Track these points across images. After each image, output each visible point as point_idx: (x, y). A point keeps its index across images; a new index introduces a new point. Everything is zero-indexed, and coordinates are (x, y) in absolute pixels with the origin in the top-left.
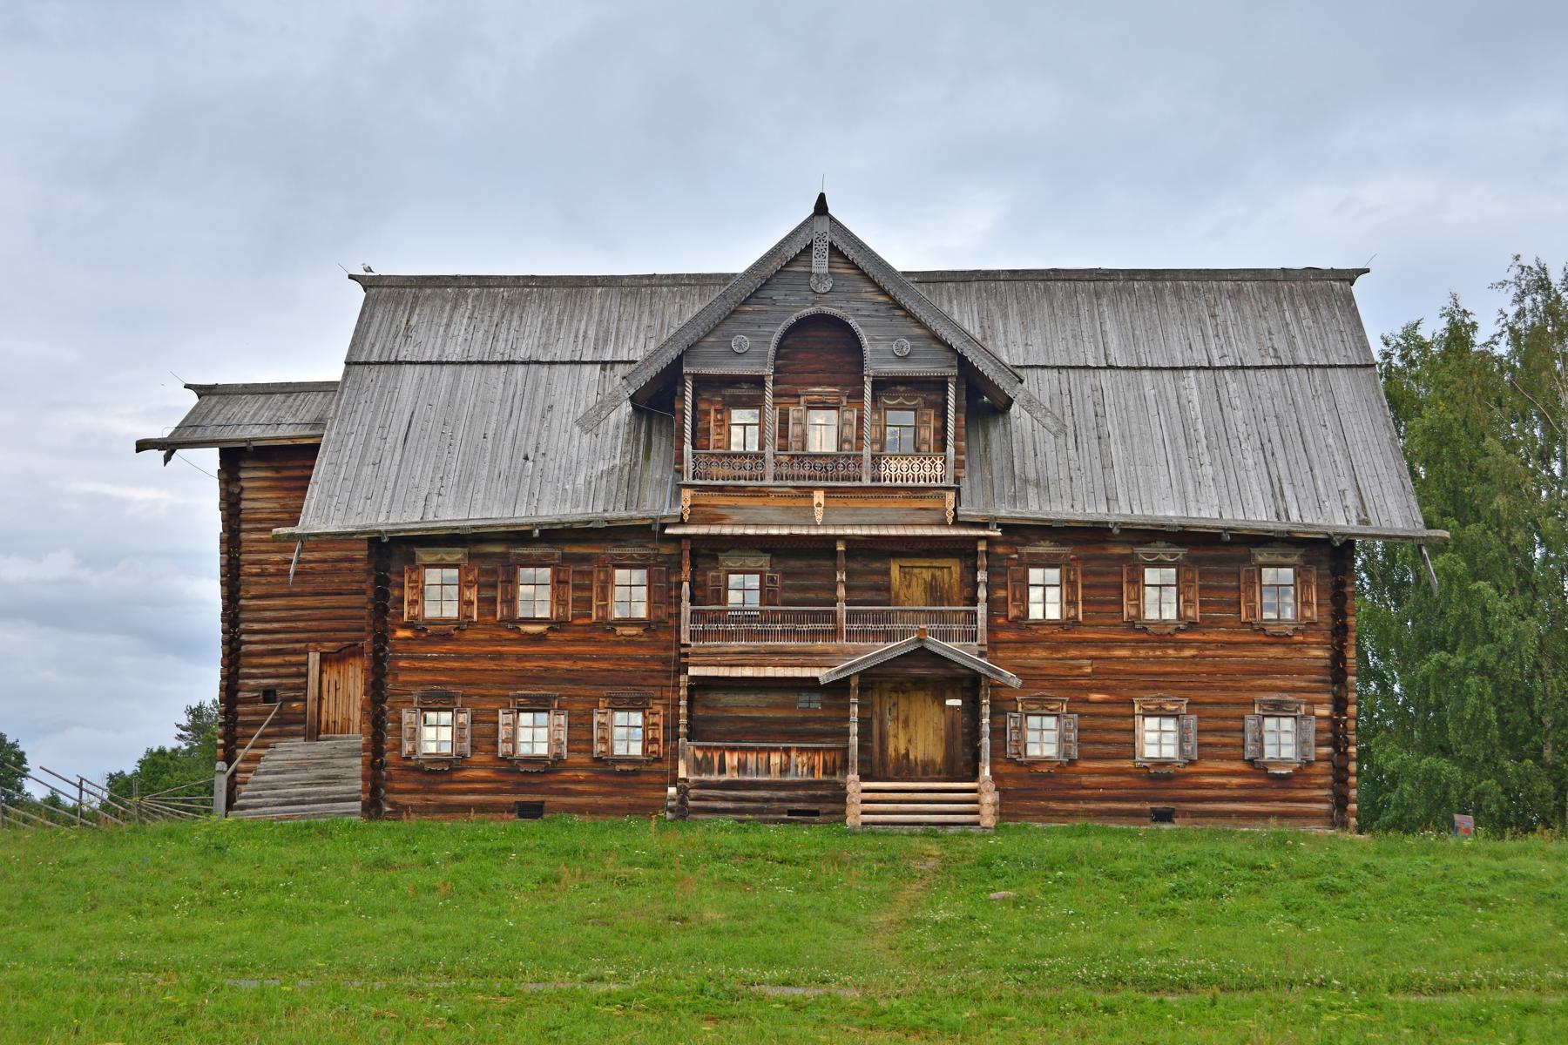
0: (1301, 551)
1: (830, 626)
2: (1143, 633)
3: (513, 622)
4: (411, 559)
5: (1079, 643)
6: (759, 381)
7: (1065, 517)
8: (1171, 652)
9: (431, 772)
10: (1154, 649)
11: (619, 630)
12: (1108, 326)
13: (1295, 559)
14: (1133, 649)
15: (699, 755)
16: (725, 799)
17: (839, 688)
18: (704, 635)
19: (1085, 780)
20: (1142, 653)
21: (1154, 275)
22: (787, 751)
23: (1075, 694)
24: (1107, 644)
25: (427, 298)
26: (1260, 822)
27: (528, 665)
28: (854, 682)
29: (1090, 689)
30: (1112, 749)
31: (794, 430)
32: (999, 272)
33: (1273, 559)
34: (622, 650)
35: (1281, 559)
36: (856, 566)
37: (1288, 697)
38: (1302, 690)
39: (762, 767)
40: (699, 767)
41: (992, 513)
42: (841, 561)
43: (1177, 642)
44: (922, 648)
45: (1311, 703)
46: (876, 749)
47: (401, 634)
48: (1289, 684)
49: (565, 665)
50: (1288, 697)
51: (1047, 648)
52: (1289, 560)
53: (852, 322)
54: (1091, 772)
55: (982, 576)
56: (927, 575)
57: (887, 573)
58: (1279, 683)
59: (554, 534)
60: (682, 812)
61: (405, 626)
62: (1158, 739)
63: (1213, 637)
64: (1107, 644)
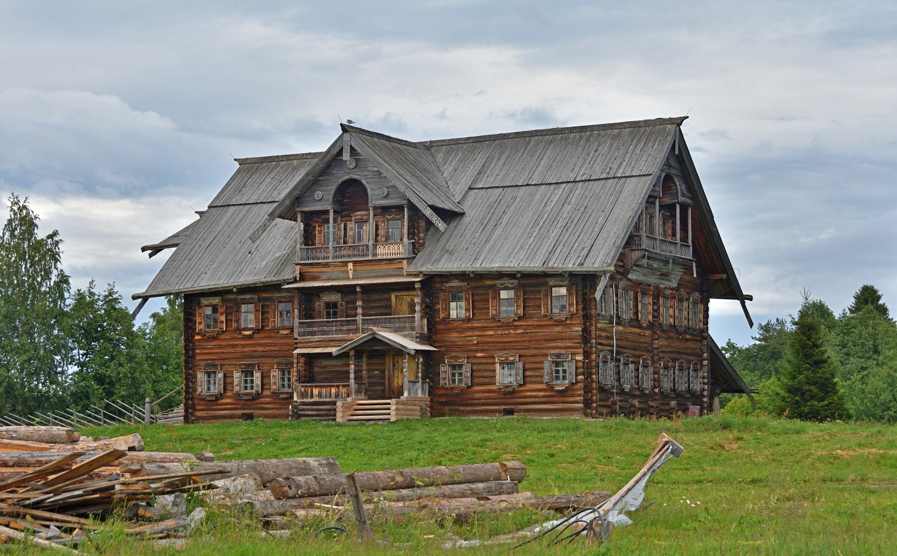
1: (354, 327)
2: (499, 323)
3: (239, 330)
4: (199, 304)
5: (473, 328)
7: (449, 270)
9: (209, 401)
10: (504, 330)
11: (281, 332)
13: (566, 283)
14: (496, 330)
15: (303, 390)
16: (312, 410)
17: (344, 355)
18: (304, 334)
20: (499, 332)
22: (338, 386)
23: (471, 354)
24: (484, 328)
25: (263, 168)
27: (246, 350)
28: (352, 353)
29: (477, 351)
30: (487, 380)
32: (510, 134)
33: (556, 283)
34: (283, 341)
35: (560, 283)
37: (563, 351)
38: (571, 348)
39: (328, 394)
40: (303, 395)
41: (420, 270)
42: (359, 296)
43: (515, 326)
44: (374, 337)
45: (573, 354)
46: (387, 384)
47: (197, 337)
48: (564, 345)
49: (260, 349)
50: (563, 351)
52: (564, 283)
54: (478, 392)
56: (409, 299)
57: (390, 299)
58: (560, 345)
60: (297, 416)
61: (199, 334)
62: (505, 377)
63: (530, 323)
64: (484, 328)
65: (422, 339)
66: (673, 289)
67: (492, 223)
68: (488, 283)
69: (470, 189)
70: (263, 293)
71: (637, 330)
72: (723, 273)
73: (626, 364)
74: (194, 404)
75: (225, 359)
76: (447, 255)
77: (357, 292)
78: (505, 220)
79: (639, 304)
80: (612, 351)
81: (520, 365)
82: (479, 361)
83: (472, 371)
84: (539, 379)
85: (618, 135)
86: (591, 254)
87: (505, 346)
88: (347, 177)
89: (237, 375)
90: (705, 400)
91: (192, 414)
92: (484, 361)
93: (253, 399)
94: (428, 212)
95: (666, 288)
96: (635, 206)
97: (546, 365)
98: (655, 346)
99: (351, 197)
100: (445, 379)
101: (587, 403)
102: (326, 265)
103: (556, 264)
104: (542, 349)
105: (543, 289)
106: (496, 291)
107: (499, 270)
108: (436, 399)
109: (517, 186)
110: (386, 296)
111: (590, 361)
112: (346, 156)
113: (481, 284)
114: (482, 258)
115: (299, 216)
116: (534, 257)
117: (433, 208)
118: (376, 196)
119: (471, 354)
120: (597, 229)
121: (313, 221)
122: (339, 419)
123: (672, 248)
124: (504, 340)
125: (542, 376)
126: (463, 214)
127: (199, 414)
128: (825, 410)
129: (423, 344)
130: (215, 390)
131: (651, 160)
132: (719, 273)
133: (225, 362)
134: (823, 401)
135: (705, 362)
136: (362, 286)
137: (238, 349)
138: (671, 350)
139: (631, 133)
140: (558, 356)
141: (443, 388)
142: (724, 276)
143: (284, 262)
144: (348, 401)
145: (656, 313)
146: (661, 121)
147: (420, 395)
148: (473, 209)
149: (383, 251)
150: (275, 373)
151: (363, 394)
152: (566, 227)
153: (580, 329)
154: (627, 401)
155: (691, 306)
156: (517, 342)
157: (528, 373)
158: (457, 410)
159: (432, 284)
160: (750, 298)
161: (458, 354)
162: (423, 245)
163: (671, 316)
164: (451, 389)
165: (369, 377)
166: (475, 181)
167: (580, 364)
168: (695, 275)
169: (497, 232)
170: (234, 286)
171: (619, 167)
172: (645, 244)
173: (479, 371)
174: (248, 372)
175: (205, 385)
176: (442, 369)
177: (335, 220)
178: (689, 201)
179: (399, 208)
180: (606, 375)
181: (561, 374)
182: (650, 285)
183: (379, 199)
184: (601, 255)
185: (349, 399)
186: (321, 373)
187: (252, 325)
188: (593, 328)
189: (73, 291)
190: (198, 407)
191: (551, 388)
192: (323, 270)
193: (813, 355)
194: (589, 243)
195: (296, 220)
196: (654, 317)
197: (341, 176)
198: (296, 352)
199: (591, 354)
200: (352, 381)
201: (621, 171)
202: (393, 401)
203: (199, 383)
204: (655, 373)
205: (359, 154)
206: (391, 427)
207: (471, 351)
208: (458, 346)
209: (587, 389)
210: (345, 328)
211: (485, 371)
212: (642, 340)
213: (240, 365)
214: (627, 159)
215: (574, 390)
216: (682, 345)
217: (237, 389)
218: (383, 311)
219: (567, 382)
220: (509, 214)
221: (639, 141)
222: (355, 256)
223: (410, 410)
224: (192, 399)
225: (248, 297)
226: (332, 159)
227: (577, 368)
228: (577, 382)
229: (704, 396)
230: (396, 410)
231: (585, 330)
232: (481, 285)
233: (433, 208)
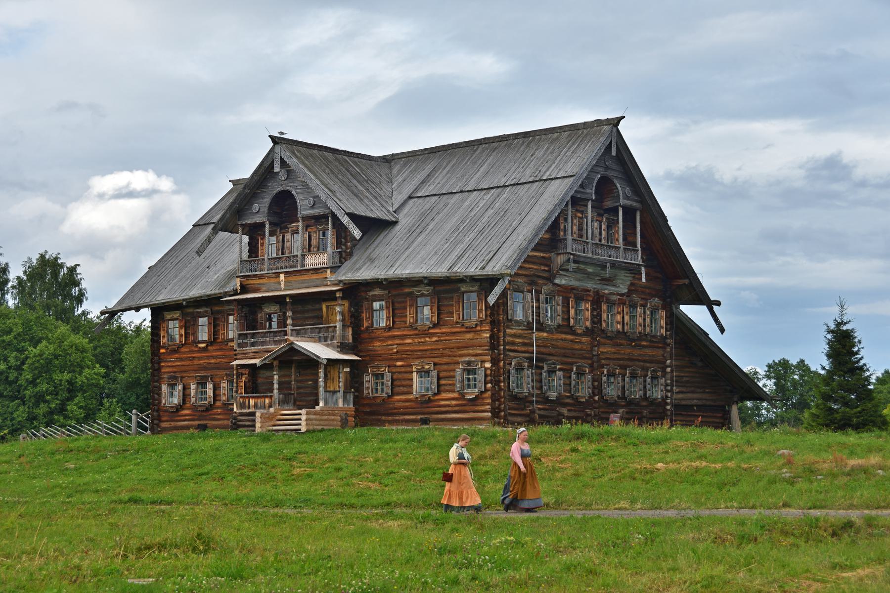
0: (478, 284)
5: (394, 337)
7: (365, 278)
8: (427, 339)
13: (476, 288)
14: (413, 339)
19: (397, 405)
20: (416, 340)
21: (526, 135)
23: (391, 363)
27: (202, 362)
28: (276, 363)
29: (397, 360)
31: (287, 244)
37: (473, 359)
40: (242, 406)
45: (483, 362)
47: (162, 351)
49: (213, 361)
50: (473, 359)
53: (293, 192)
54: (399, 401)
57: (321, 309)
58: (471, 352)
59: (433, 282)
61: (163, 347)
62: (419, 385)
63: (444, 330)
66: (622, 295)
67: (418, 230)
70: (211, 305)
71: (569, 337)
72: (685, 278)
73: (551, 372)
74: (159, 416)
75: (185, 371)
76: (369, 263)
77: (299, 302)
78: (430, 227)
79: (597, 308)
80: (531, 359)
81: (434, 373)
82: (399, 370)
85: (558, 138)
86: (495, 258)
87: (422, 355)
89: (193, 387)
90: (668, 407)
92: (403, 369)
94: (345, 220)
95: (610, 294)
97: (458, 373)
99: (284, 210)
100: (368, 388)
101: (495, 413)
102: (262, 277)
103: (461, 269)
104: (455, 356)
105: (455, 295)
106: (413, 297)
107: (408, 276)
109: (452, 193)
110: (317, 306)
112: (277, 168)
116: (443, 262)
118: (304, 208)
119: (391, 363)
121: (255, 232)
123: (612, 252)
124: (421, 348)
125: (454, 385)
127: (164, 425)
130: (176, 401)
131: (578, 161)
135: (669, 369)
136: (291, 296)
137: (196, 362)
138: (619, 356)
139: (569, 135)
140: (469, 363)
142: (686, 281)
143: (232, 275)
144: (265, 412)
145: (597, 318)
146: (599, 122)
147: (341, 404)
149: (312, 261)
150: (224, 384)
152: (481, 232)
153: (488, 335)
154: (554, 410)
155: (648, 312)
156: (432, 350)
157: (442, 382)
158: (379, 420)
159: (356, 293)
160: (718, 303)
161: (380, 364)
162: (351, 254)
163: (618, 323)
165: (298, 388)
166: (416, 190)
167: (489, 372)
168: (644, 280)
169: (420, 239)
170: (184, 300)
171: (548, 170)
173: (400, 379)
174: (202, 384)
175: (170, 397)
176: (366, 378)
177: (271, 234)
178: (635, 204)
179: (325, 217)
180: (524, 383)
182: (589, 291)
183: (306, 209)
185: (272, 410)
187: (206, 338)
190: (164, 419)
191: (462, 396)
192: (261, 281)
194: (498, 246)
195: (534, 250)
196: (593, 322)
197: (275, 188)
199: (499, 361)
200: (276, 391)
201: (548, 173)
202: (303, 411)
203: (163, 395)
205: (288, 166)
207: (392, 359)
209: (495, 398)
210: (277, 339)
212: (577, 346)
213: (196, 377)
214: (557, 162)
215: (483, 399)
216: (637, 352)
217: (193, 400)
219: (477, 390)
221: (573, 144)
222: (287, 267)
223: (326, 420)
224: (157, 411)
227: (486, 376)
228: (486, 390)
229: (667, 404)
230: (306, 420)
232: (398, 290)
233: (352, 216)
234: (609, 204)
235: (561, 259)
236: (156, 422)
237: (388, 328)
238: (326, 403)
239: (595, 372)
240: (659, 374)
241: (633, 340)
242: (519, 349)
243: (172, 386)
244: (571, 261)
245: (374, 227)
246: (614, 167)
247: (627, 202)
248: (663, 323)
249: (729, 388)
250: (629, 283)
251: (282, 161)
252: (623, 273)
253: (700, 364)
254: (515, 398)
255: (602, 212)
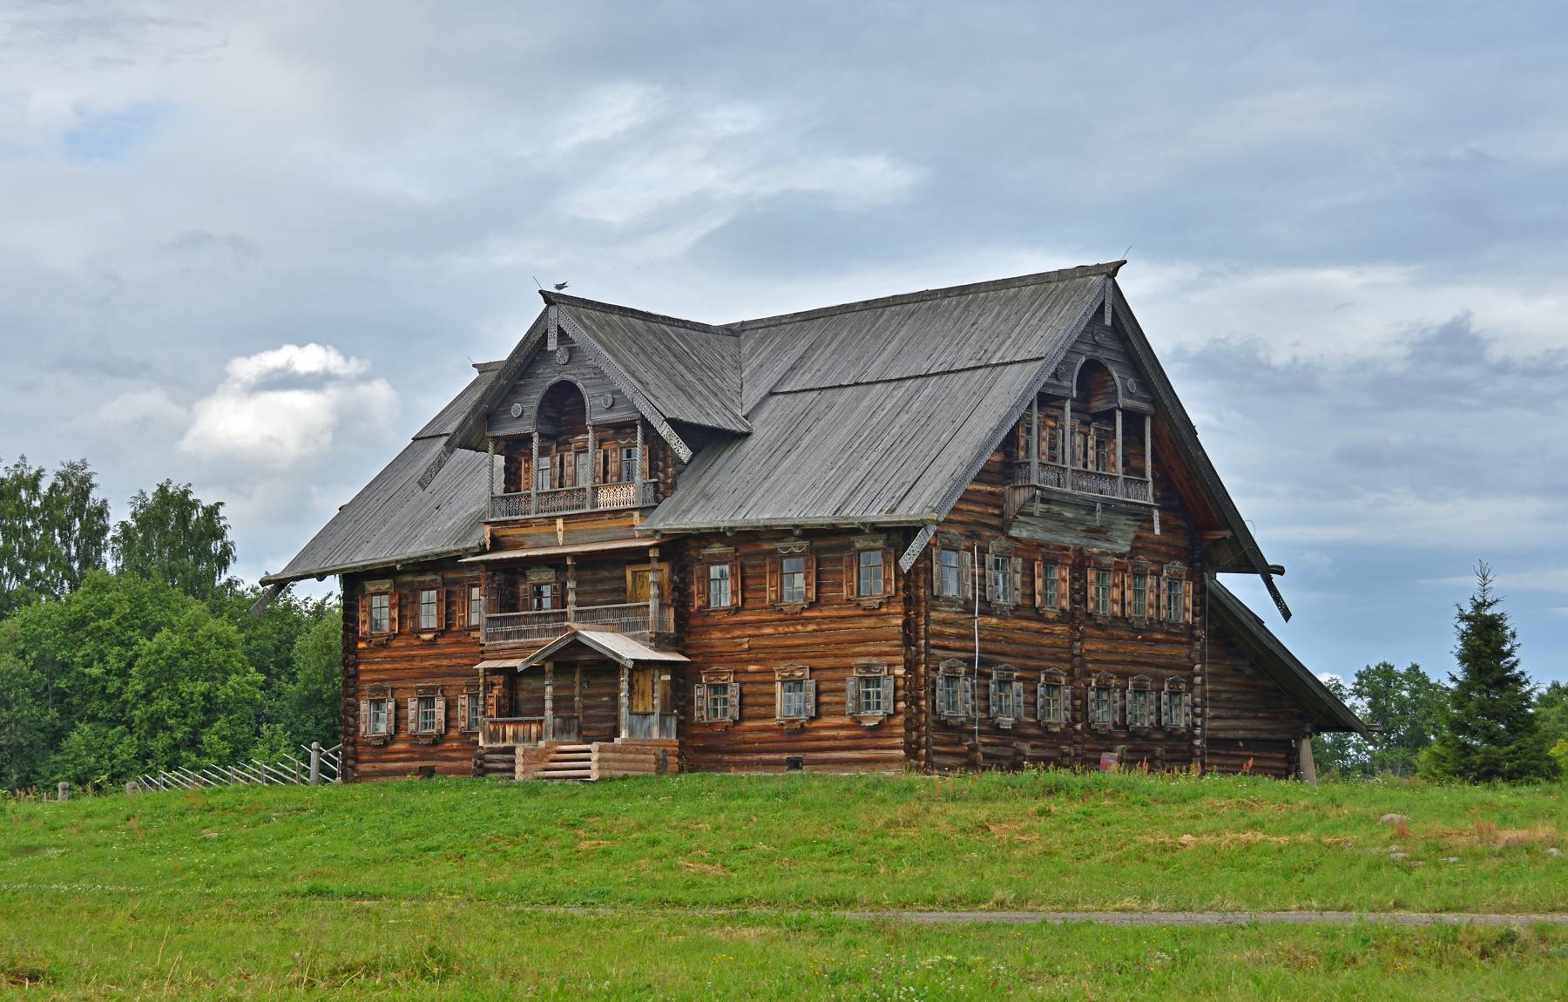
5: (744, 624)
6: (528, 438)
12: (301, 401)
14: (775, 627)
20: (781, 630)
23: (739, 667)
24: (759, 624)
26: (868, 767)
28: (548, 666)
29: (749, 662)
30: (763, 711)
31: (568, 470)
36: (588, 575)
37: (875, 661)
40: (492, 737)
45: (891, 665)
47: (361, 645)
49: (445, 662)
50: (875, 661)
51: (721, 631)
53: (579, 384)
54: (751, 730)
55: (571, 585)
57: (624, 577)
58: (871, 649)
61: (363, 640)
62: (787, 704)
64: (759, 624)
65: (659, 642)
66: (1122, 556)
67: (785, 448)
68: (766, 547)
69: (772, 394)
75: (398, 679)
78: (804, 443)
80: (970, 662)
81: (810, 685)
82: (751, 678)
83: (742, 696)
84: (839, 708)
86: (912, 493)
88: (555, 379)
89: (412, 705)
91: (353, 767)
92: (758, 678)
93: (435, 743)
96: (1003, 411)
97: (850, 684)
98: (1076, 652)
99: (563, 411)
101: (912, 750)
102: (526, 523)
103: (855, 513)
104: (845, 656)
105: (845, 555)
108: (689, 742)
109: (840, 386)
110: (617, 573)
111: (917, 676)
112: (552, 345)
113: (755, 549)
114: (750, 505)
115: (491, 445)
117: (675, 424)
118: (597, 411)
119: (739, 667)
120: (934, 452)
121: (514, 449)
122: (518, 776)
123: (1105, 485)
124: (789, 642)
125: (843, 703)
126: (747, 435)
127: (363, 767)
128: (1510, 760)
129: (665, 651)
131: (1050, 335)
132: (1219, 529)
133: (398, 685)
134: (1509, 744)
136: (574, 556)
137: (416, 664)
138: (1116, 658)
139: (1035, 291)
140: (868, 667)
141: (699, 725)
142: (1228, 534)
146: (1083, 271)
147: (655, 735)
148: (763, 431)
149: (609, 498)
151: (574, 734)
153: (900, 622)
154: (1009, 745)
155: (1164, 585)
156: (807, 645)
158: (719, 762)
159: (680, 550)
160: (1280, 571)
162: (673, 487)
163: (1115, 602)
164: (711, 725)
166: (781, 381)
167: (901, 683)
168: (1157, 531)
170: (398, 561)
171: (999, 348)
172: (1036, 476)
173: (753, 694)
174: (427, 700)
175: (374, 722)
176: (698, 692)
178: (1144, 406)
179: (631, 425)
180: (960, 702)
181: (874, 700)
182: (1066, 549)
184: (927, 493)
185: (542, 744)
186: (528, 700)
187: (433, 624)
188: (922, 620)
189: (229, 575)
192: (524, 531)
193: (1492, 669)
196: (1073, 601)
197: (548, 377)
198: (481, 666)
199: (918, 664)
200: (549, 713)
201: (999, 354)
202: (594, 746)
203: (362, 718)
204: (1074, 697)
205: (571, 341)
206: (588, 788)
208: (721, 654)
209: (911, 725)
210: (550, 626)
211: (762, 694)
212: (1046, 641)
215: (892, 727)
216: (1144, 650)
217: (412, 727)
218: (614, 597)
219: (881, 712)
220: (814, 432)
221: (1041, 306)
222: (568, 508)
223: (631, 761)
224: (353, 744)
225: (428, 578)
226: (533, 351)
227: (896, 689)
228: (897, 713)
230: (599, 760)
231: (906, 624)
232: (752, 546)
233: (675, 424)
234: (1099, 405)
235: (1021, 496)
236: (350, 762)
237: (735, 610)
238: (631, 733)
239: (1077, 684)
240: (1182, 687)
241: (1139, 631)
242: (951, 644)
243: (377, 704)
244: (1038, 500)
245: (711, 441)
246: (1109, 343)
247: (1130, 403)
248: (1189, 602)
249: (1296, 711)
250: (1132, 536)
251: (561, 333)
252: (1123, 519)
253: (1249, 671)
254: (943, 726)
255: (1088, 418)
